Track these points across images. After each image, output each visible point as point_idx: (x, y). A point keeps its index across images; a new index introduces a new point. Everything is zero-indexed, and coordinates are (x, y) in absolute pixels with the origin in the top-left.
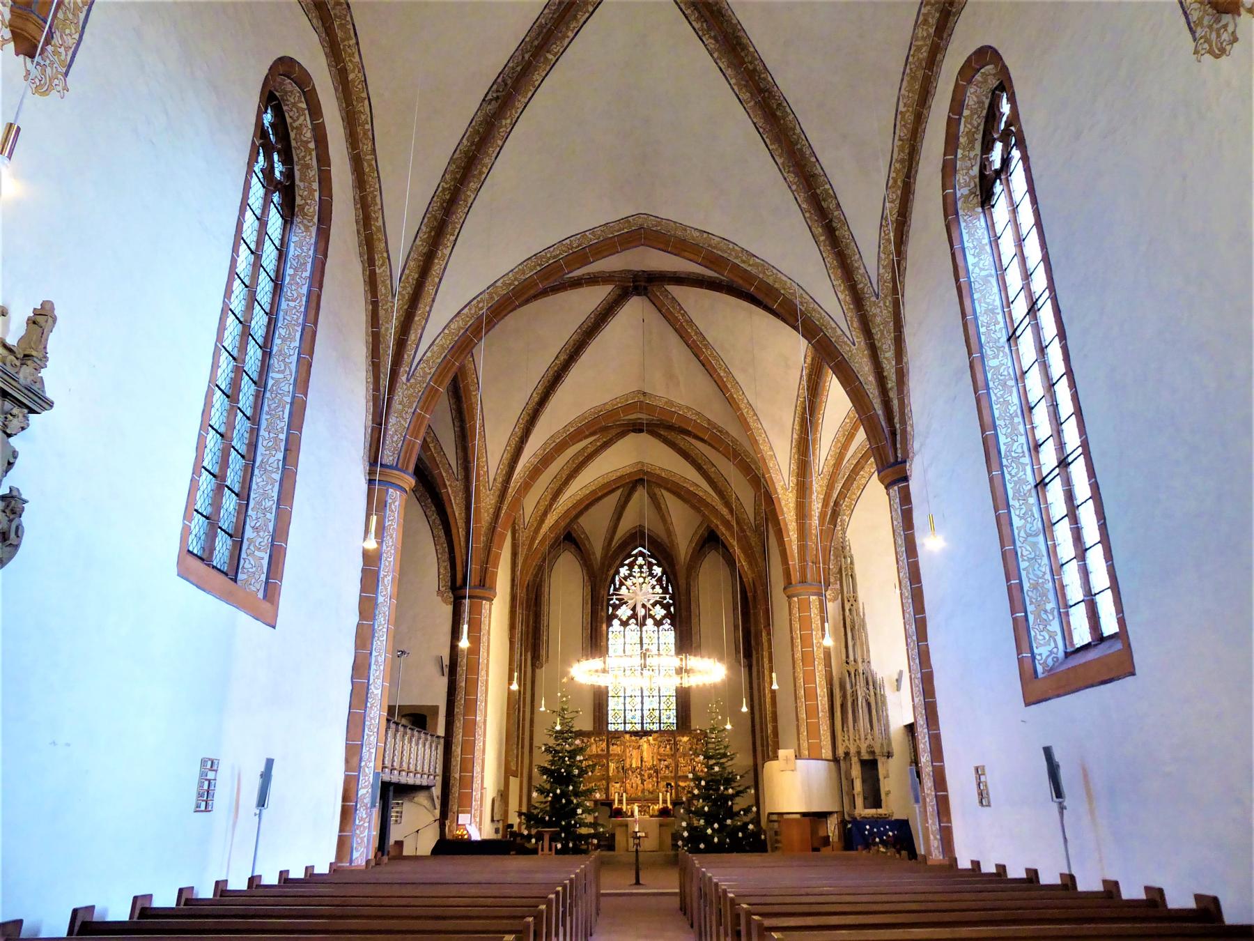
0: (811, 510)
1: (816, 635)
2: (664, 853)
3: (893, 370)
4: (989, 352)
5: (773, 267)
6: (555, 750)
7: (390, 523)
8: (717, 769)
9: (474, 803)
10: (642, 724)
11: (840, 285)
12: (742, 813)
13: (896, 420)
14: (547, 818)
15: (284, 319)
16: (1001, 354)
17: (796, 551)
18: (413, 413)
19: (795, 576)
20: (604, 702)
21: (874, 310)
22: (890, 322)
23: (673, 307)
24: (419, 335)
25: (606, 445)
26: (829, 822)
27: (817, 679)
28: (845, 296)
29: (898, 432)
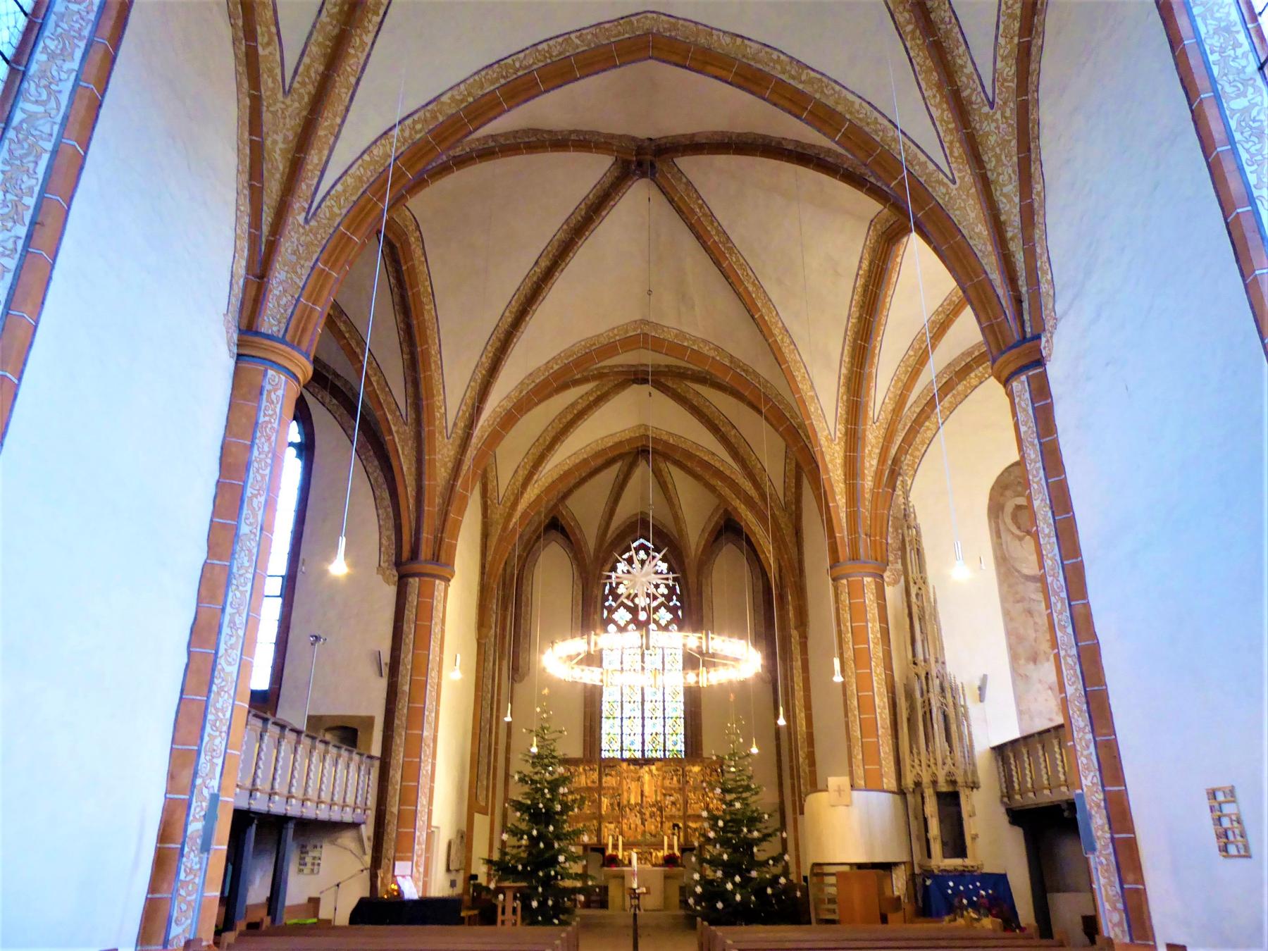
0: (863, 467)
1: (872, 628)
2: (668, 912)
3: (1016, 210)
4: (1228, 89)
5: (836, 82)
6: (532, 780)
7: (267, 419)
8: (738, 805)
9: (416, 847)
10: (643, 751)
11: (934, 96)
12: (771, 862)
13: (1022, 282)
14: (520, 867)
15: (57, 26)
16: (1251, 90)
17: (844, 520)
18: (312, 268)
19: (844, 552)
20: (598, 712)
21: (988, 127)
22: (1010, 141)
23: (688, 195)
24: (324, 158)
25: (599, 399)
26: (894, 876)
27: (875, 684)
28: (943, 113)
29: (1025, 298)
